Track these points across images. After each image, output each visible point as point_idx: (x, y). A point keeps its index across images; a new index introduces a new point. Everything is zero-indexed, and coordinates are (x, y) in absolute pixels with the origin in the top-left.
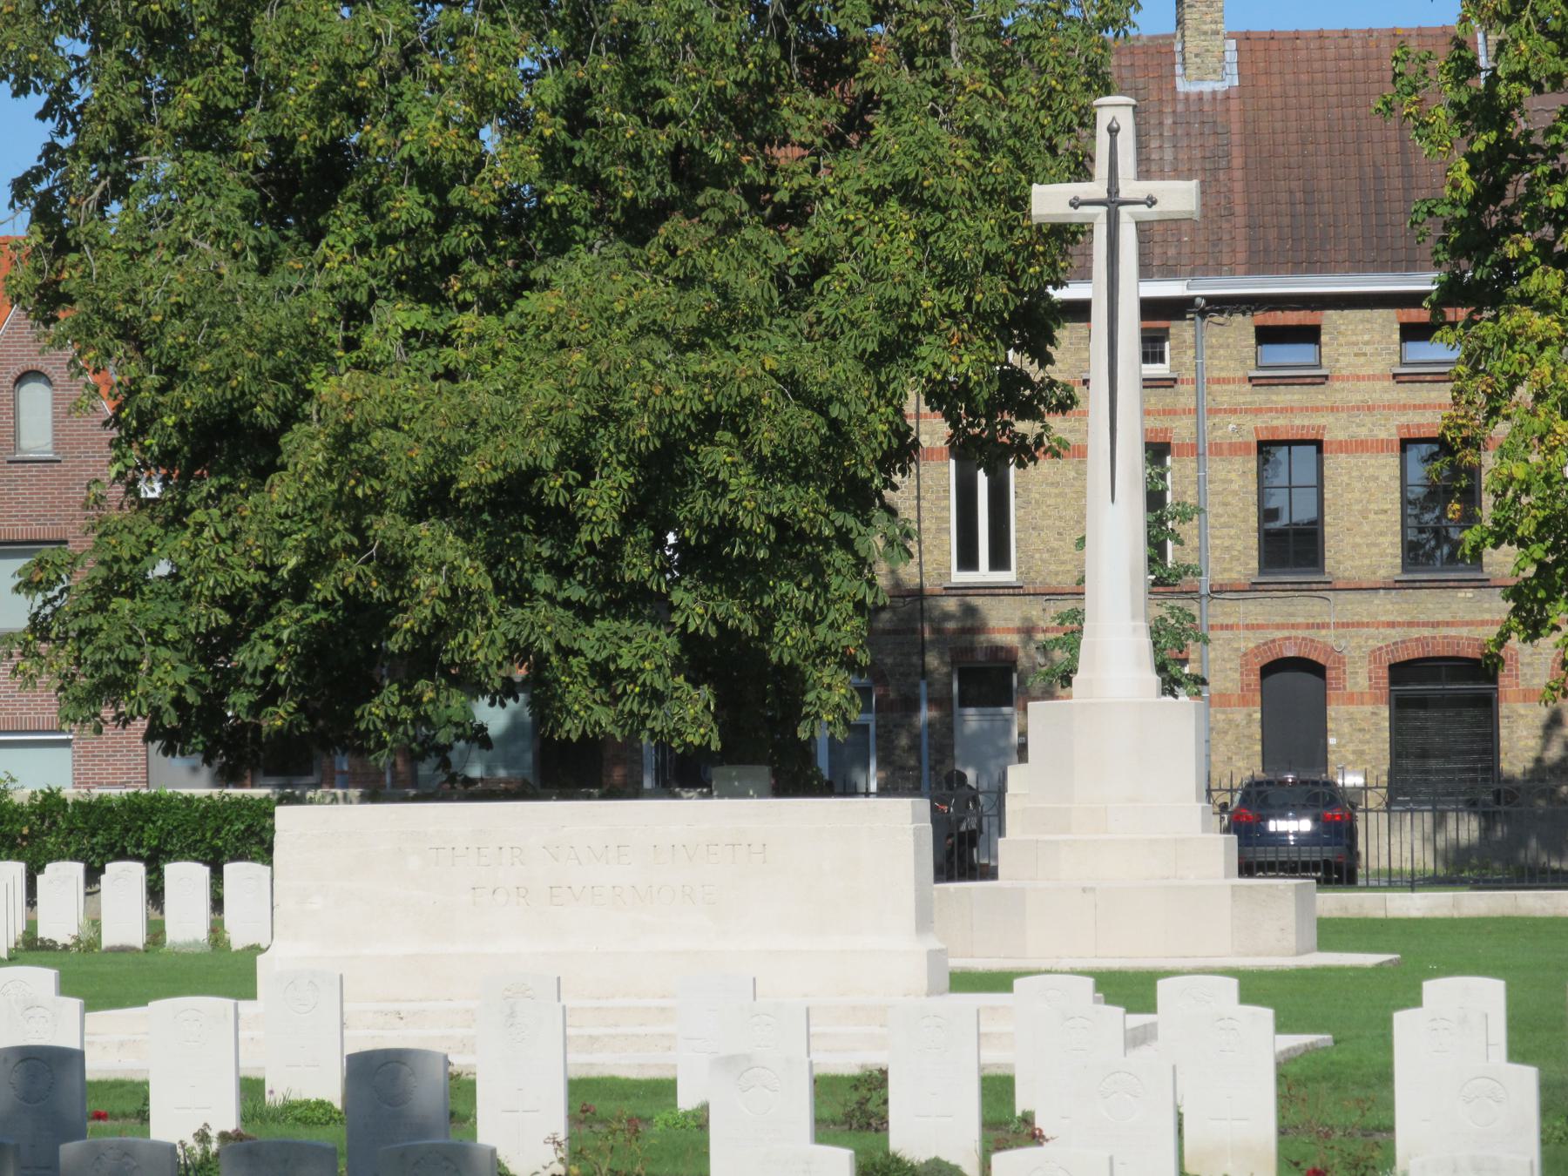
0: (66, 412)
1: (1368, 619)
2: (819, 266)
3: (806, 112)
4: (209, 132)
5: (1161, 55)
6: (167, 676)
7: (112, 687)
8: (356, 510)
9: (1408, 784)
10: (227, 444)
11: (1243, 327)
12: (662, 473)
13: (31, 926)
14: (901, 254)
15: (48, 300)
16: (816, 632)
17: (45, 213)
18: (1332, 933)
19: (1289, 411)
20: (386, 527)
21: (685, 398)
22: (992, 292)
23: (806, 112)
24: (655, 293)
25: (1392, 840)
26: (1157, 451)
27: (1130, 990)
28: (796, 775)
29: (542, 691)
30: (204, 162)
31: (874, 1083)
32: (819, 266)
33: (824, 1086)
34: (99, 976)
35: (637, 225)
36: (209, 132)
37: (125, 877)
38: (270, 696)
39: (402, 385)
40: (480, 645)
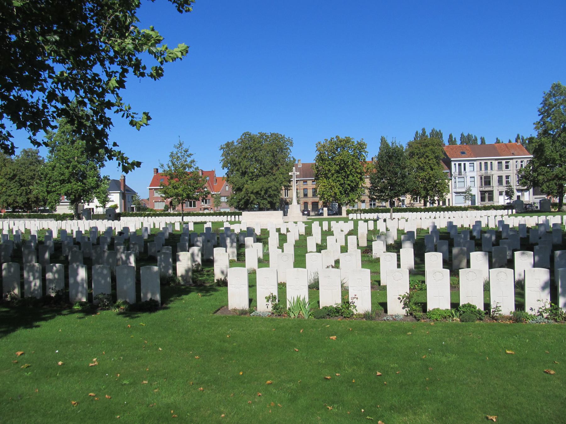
0: (229, 188)
3: (275, 168)
4: (238, 170)
5: (297, 165)
6: (235, 204)
7: (232, 205)
8: (247, 194)
9: (313, 210)
12: (266, 191)
15: (228, 181)
16: (276, 200)
17: (228, 175)
18: (308, 219)
19: (305, 187)
20: (249, 195)
22: (287, 179)
23: (275, 168)
26: (297, 189)
27: (296, 223)
28: (275, 209)
29: (259, 205)
34: (231, 223)
35: (265, 176)
36: (238, 170)
37: (233, 217)
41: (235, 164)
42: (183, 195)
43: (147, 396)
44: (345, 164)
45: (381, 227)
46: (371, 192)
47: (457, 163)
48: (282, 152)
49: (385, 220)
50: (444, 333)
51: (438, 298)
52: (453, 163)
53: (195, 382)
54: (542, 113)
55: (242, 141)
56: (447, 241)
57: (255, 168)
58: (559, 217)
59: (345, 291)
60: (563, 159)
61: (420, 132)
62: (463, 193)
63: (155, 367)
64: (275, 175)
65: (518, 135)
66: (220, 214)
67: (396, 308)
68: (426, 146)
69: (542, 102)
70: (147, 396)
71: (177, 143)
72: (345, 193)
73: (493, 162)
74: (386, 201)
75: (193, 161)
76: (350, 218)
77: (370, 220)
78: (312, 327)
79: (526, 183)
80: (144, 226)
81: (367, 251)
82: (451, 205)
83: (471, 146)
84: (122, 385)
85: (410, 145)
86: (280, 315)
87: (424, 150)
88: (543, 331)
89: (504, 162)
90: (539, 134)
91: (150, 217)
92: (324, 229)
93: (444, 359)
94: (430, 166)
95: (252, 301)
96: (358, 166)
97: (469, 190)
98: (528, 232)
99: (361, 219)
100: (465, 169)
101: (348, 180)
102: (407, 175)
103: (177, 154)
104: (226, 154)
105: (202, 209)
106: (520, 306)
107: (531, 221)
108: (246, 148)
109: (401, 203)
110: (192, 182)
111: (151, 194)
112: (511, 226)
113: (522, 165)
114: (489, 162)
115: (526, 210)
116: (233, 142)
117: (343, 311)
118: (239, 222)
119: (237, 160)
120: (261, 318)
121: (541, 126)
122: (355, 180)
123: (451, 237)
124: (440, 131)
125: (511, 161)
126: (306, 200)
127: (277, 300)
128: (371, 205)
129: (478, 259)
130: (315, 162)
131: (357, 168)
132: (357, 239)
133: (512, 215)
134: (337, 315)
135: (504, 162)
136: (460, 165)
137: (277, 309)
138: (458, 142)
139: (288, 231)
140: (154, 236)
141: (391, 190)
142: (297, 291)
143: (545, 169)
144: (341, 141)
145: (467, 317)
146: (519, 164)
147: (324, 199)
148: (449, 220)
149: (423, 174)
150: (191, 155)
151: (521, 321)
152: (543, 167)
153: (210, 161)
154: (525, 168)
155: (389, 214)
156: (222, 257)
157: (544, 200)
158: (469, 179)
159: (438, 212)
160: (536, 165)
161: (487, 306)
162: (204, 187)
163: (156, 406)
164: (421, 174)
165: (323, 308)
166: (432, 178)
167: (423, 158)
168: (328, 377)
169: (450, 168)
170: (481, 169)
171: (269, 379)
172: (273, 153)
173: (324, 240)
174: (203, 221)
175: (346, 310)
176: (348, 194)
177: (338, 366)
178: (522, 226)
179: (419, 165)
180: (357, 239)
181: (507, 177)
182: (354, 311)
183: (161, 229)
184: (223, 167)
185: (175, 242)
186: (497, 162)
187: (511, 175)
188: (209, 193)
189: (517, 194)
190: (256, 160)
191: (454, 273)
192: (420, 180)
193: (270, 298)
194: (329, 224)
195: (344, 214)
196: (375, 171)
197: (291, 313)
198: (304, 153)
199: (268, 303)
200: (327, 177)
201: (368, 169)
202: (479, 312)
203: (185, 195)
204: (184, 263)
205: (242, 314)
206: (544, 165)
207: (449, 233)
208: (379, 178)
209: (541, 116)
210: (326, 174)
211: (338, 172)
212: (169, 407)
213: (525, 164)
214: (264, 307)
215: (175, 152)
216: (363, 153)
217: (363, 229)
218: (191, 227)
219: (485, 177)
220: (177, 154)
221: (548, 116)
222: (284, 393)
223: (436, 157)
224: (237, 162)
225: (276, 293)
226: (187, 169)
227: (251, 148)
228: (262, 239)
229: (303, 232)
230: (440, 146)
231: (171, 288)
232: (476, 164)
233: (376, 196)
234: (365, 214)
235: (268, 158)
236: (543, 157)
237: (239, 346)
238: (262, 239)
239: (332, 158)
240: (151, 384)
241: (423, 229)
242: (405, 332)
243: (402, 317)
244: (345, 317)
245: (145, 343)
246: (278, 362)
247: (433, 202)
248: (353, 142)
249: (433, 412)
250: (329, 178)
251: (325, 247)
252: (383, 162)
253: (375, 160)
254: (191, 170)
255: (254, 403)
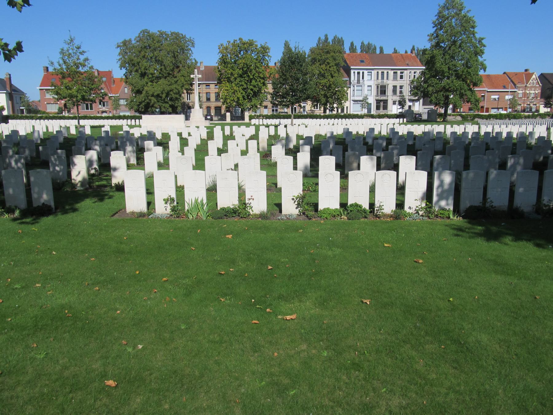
1: (213, 104)
2: (177, 81)
3: (176, 70)
4: (137, 71)
5: (199, 67)
6: (136, 107)
7: (132, 108)
8: (148, 96)
10: (139, 92)
11: (205, 85)
12: (168, 94)
13: (541, 175)
14: (183, 80)
15: (126, 82)
17: (126, 76)
18: (211, 124)
19: (208, 91)
20: (150, 97)
21: (169, 89)
22: (189, 82)
23: (176, 70)
24: (167, 82)
25: (215, 118)
26: (199, 93)
27: (198, 127)
28: (177, 113)
29: (160, 108)
30: (136, 73)
31: (181, 133)
32: (177, 81)
33: (178, 133)
34: (131, 127)
35: (166, 78)
36: (137, 71)
37: (133, 121)
38: (142, 108)
39: (150, 88)
40: (156, 105)
41: (134, 65)
42: (77, 97)
43: (41, 298)
44: (248, 68)
45: (282, 133)
46: (273, 97)
47: (356, 71)
48: (184, 53)
49: (286, 126)
50: (332, 230)
51: (328, 198)
52: (352, 71)
53: (90, 282)
54: (436, 26)
55: (139, 39)
56: (342, 146)
57: (155, 69)
58: (443, 126)
59: (242, 192)
60: (450, 72)
61: (323, 38)
62: (360, 101)
63: (49, 270)
64: (176, 77)
65: (413, 47)
66: (120, 118)
67: (290, 208)
68: (328, 52)
69: (436, 14)
70: (41, 298)
71: (67, 39)
72: (248, 98)
73: (389, 71)
74: (288, 106)
75: (86, 60)
76: (252, 124)
77: (271, 125)
78: (210, 227)
79: (417, 93)
80: (36, 129)
81: (266, 155)
82: (349, 113)
83: (372, 56)
84: (14, 289)
85: (312, 51)
86: (178, 217)
87: (326, 57)
88: (417, 227)
89: (399, 72)
90: (432, 46)
91: (42, 121)
92: (226, 134)
93: (330, 253)
94: (331, 74)
95: (150, 204)
96: (261, 71)
97: (365, 99)
98: (415, 139)
99: (263, 125)
100: (363, 78)
101: (250, 85)
102: (309, 81)
103: (68, 50)
104: (123, 53)
105: (100, 112)
106: (400, 205)
107: (418, 129)
108: (145, 47)
109: (302, 110)
110: (87, 82)
111: (43, 95)
112: (400, 134)
113: (415, 76)
114: (385, 72)
115: (416, 119)
116: (130, 40)
117: (240, 211)
118: (140, 126)
119: (136, 60)
120: (159, 219)
121: (434, 38)
122: (258, 85)
123: (346, 143)
124: (342, 38)
125: (405, 72)
126: (208, 104)
127: (175, 203)
128: (273, 110)
129: (367, 163)
130: (217, 65)
131: (259, 73)
132: (258, 144)
133: (403, 123)
134: (234, 215)
135: (399, 72)
136: (359, 73)
137: (176, 211)
138: (359, 51)
139: (189, 135)
140: (48, 140)
141: (293, 96)
142: (196, 193)
143: (434, 81)
144: (244, 44)
145: (353, 216)
146: (413, 75)
147: (227, 103)
148: (346, 127)
149: (324, 81)
150: (84, 52)
151: (400, 219)
152: (433, 79)
153: (105, 60)
154: (417, 79)
155: (290, 120)
156: (117, 159)
157: (432, 110)
158: (366, 88)
159: (336, 119)
160: (427, 77)
161: (372, 205)
162: (100, 88)
163: (50, 308)
164: (322, 82)
165: (221, 209)
166: (332, 86)
167: (324, 65)
168: (223, 273)
169: (349, 76)
170: (378, 79)
171: (165, 277)
172: (174, 54)
173: (225, 144)
174: (102, 124)
175: (244, 211)
176: (251, 99)
177: (233, 262)
178: (410, 133)
179: (320, 72)
180: (258, 144)
181: (401, 87)
182: (250, 211)
183: (55, 133)
184: (121, 67)
185: (71, 146)
186: (392, 72)
187: (405, 85)
188: (106, 95)
189: (408, 103)
190: (156, 61)
191: (344, 176)
192: (321, 87)
193: (168, 200)
194: (231, 129)
195: (247, 120)
196: (277, 76)
197: (189, 215)
198: (206, 55)
199: (166, 205)
200: (229, 81)
201: (271, 74)
202: (365, 211)
203: (80, 97)
204: (80, 169)
205: (140, 216)
206: (434, 77)
207: (345, 139)
208: (281, 83)
209: (435, 28)
210: (228, 78)
211: (241, 76)
212: (63, 307)
213: (417, 75)
214: (162, 209)
215: (65, 49)
216: (267, 58)
217: (264, 134)
218: (88, 131)
219: (382, 87)
220: (68, 50)
221: (441, 29)
222: (179, 288)
223: (337, 65)
224: (136, 62)
225: (174, 195)
226: (81, 68)
227: (150, 47)
228: (163, 143)
229: (204, 136)
230: (340, 53)
231: (67, 196)
232: (374, 73)
233: (278, 101)
234: (268, 120)
235: (169, 58)
236: (434, 69)
237: (136, 247)
238: (163, 143)
239: (235, 62)
240: (44, 287)
241: (321, 135)
242: (296, 229)
243: (295, 216)
244: (242, 217)
245: (37, 248)
246: (175, 260)
247: (332, 109)
248: (256, 46)
249: (316, 299)
250: (232, 82)
251: (226, 151)
252: (285, 67)
253: (278, 65)
254: (86, 69)
255: (149, 299)
